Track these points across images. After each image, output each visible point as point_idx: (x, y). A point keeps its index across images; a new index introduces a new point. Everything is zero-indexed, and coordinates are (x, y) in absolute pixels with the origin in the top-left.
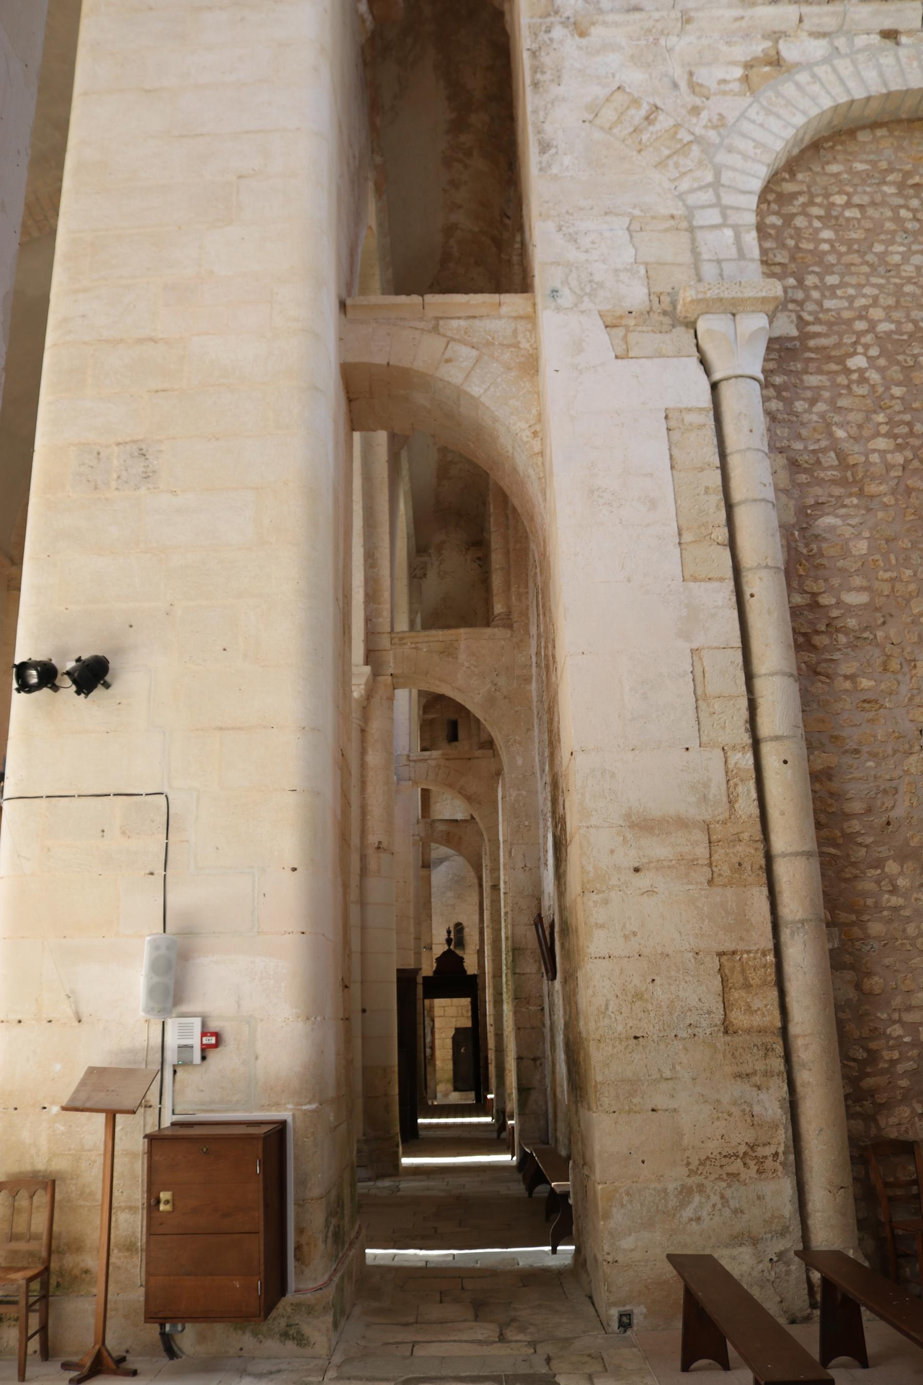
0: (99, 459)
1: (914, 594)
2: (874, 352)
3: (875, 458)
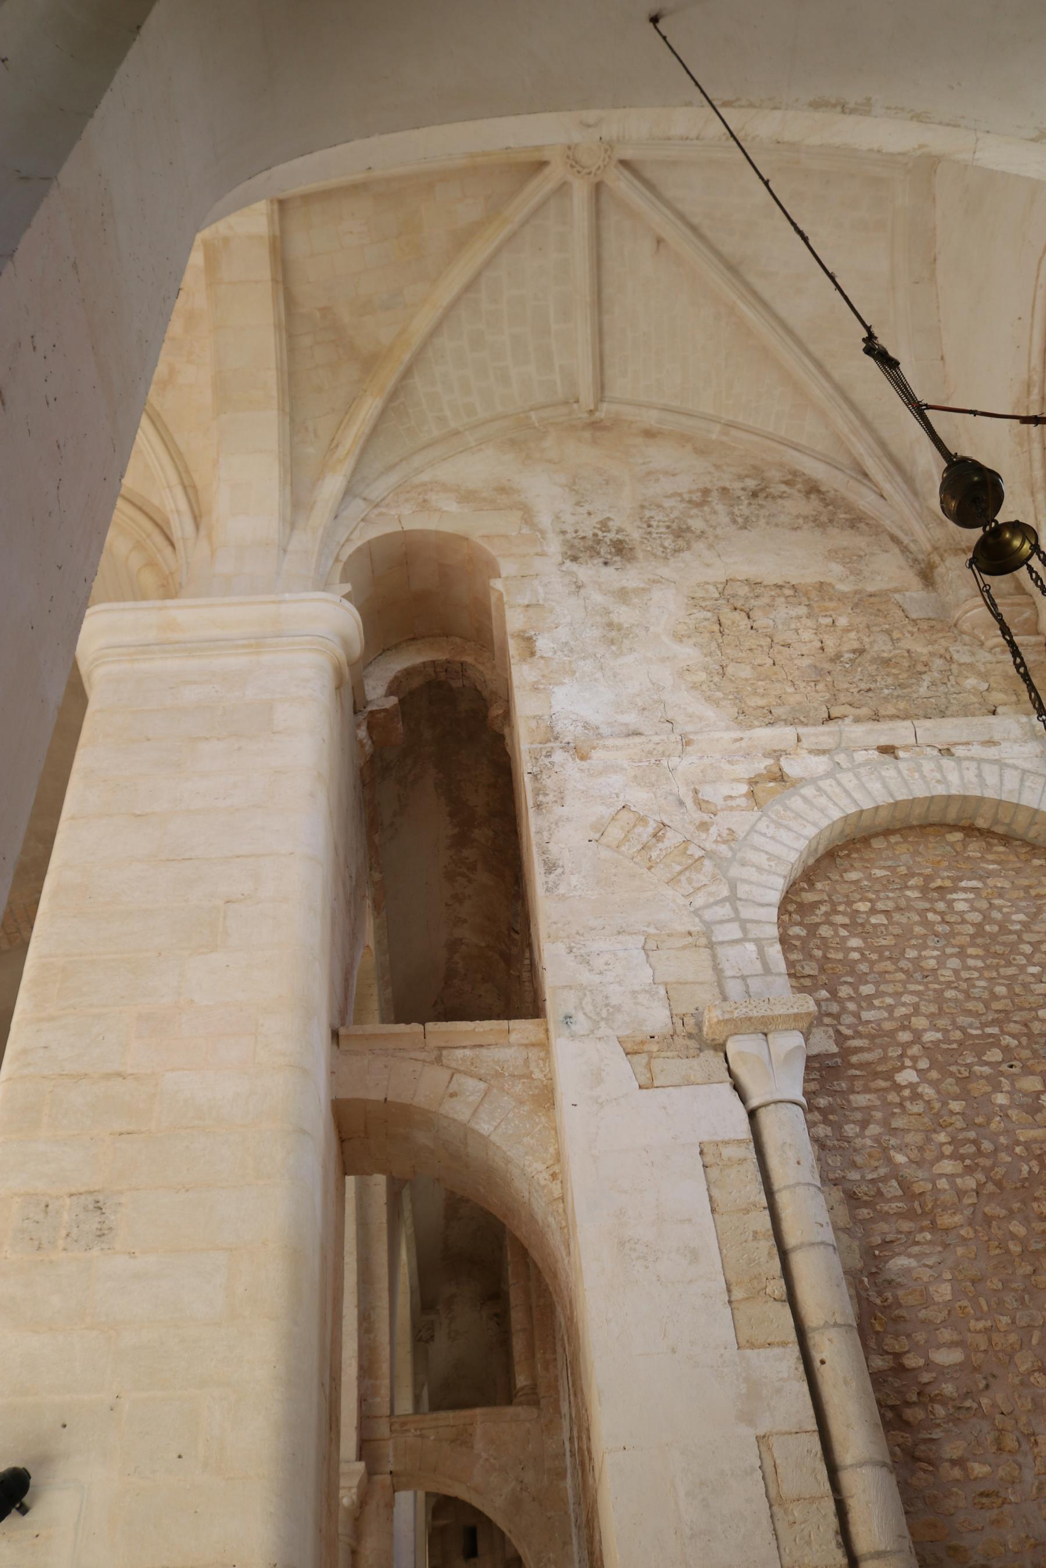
0: (46, 1213)
1: (1017, 1347)
2: (924, 1064)
3: (943, 1184)
